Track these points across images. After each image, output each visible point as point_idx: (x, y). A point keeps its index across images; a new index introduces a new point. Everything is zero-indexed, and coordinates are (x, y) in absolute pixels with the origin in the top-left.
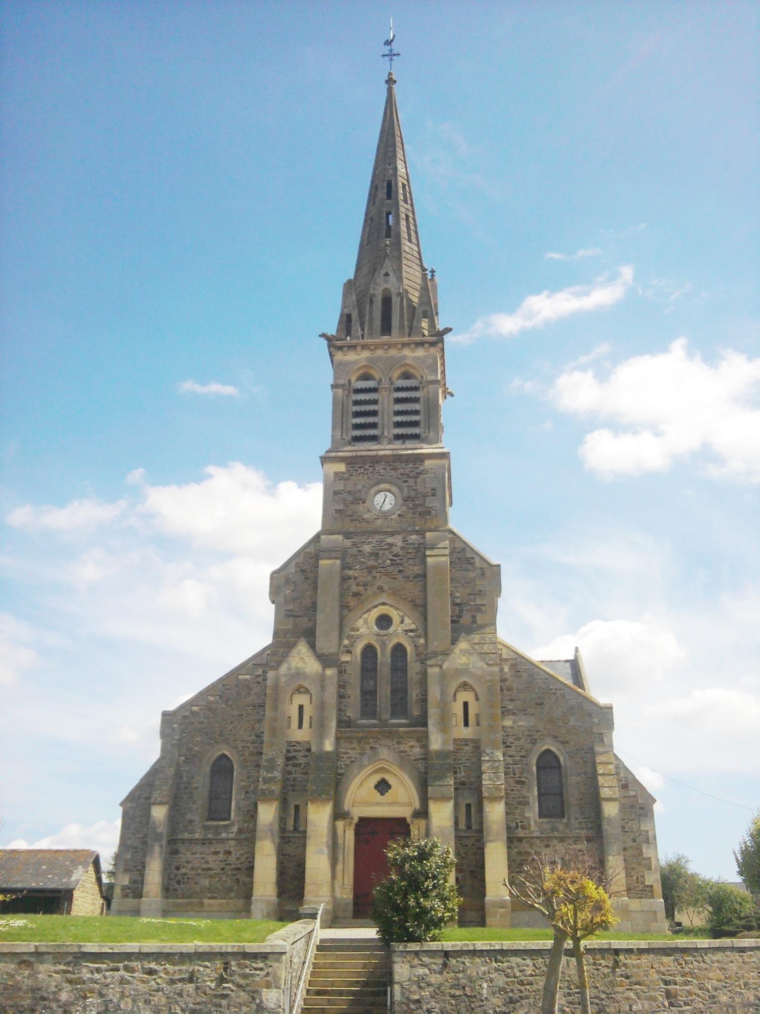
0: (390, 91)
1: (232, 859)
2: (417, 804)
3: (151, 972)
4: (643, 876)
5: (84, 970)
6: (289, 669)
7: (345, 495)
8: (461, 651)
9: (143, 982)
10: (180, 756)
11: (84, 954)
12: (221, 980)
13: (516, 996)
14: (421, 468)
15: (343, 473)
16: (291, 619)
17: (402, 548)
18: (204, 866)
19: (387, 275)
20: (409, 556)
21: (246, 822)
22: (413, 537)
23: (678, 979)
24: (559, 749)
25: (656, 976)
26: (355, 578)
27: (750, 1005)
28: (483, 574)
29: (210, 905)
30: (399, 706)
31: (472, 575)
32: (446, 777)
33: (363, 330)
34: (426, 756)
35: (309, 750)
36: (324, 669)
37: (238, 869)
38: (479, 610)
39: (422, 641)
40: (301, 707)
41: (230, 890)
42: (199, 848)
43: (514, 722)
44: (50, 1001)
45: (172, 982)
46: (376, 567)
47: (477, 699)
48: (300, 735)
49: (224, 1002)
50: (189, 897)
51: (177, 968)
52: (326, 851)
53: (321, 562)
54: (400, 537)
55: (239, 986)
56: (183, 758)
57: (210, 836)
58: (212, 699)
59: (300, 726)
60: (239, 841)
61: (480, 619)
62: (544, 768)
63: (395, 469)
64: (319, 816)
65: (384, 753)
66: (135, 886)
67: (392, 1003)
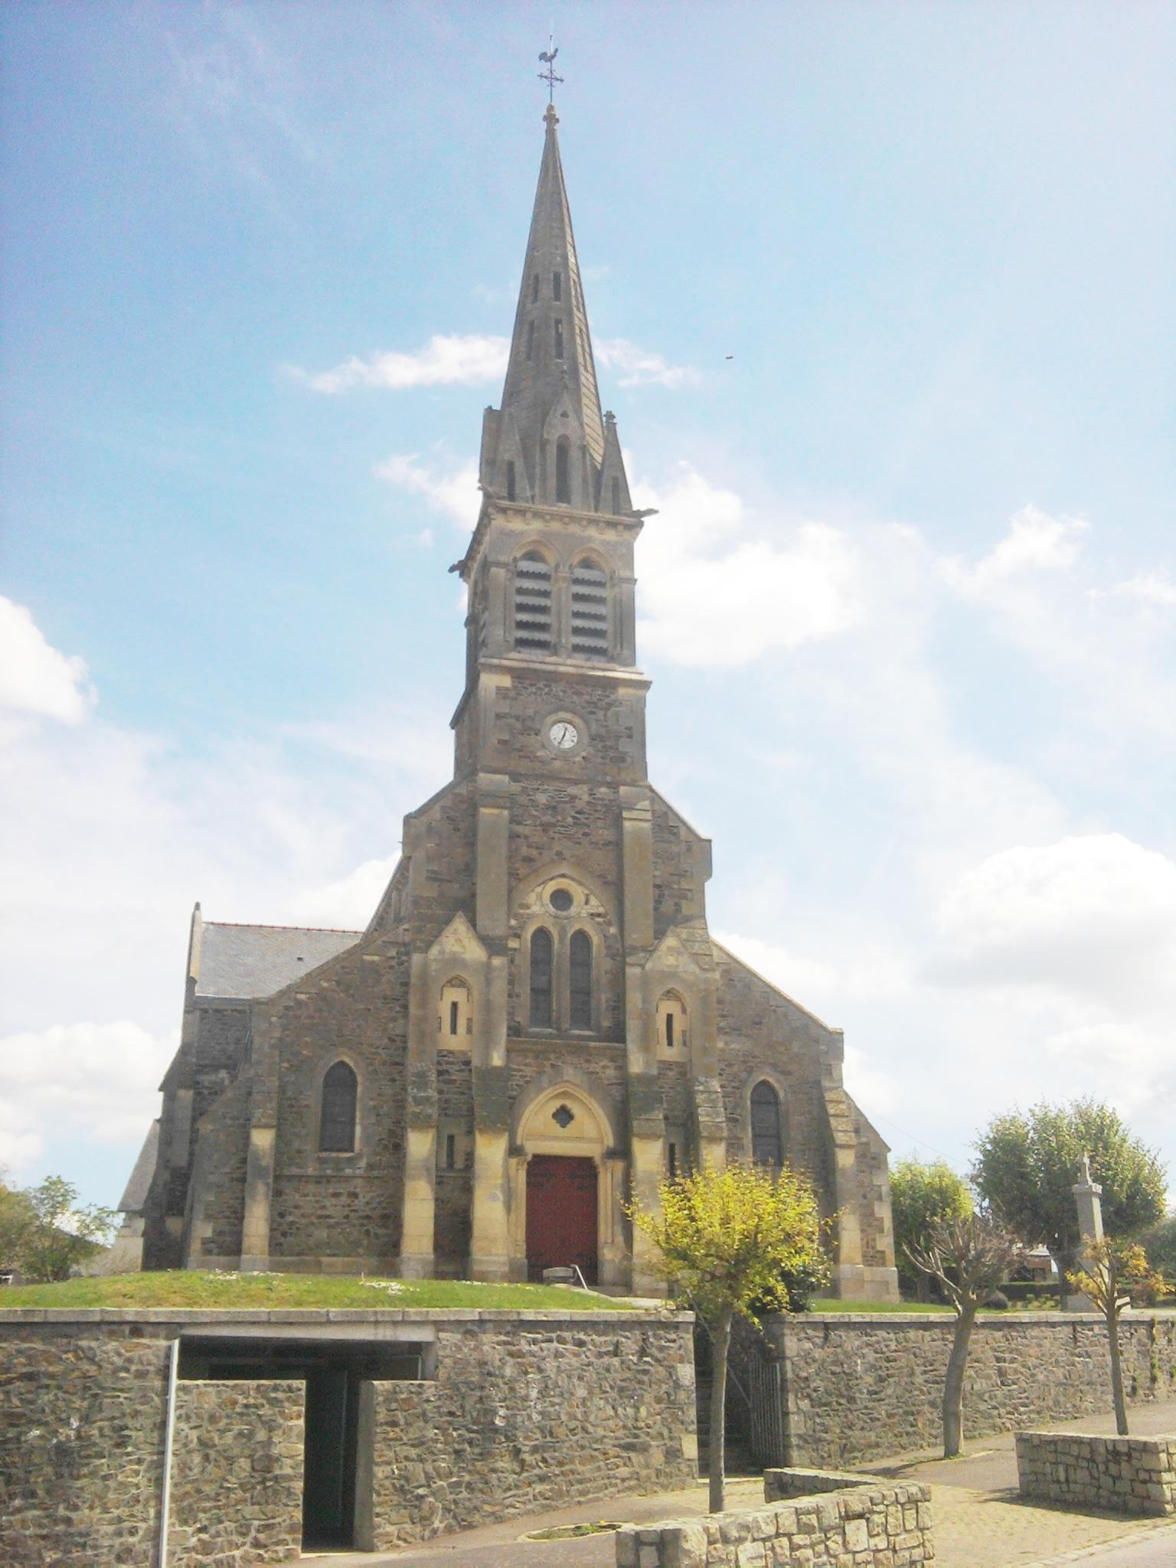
0: (551, 134)
1: (360, 1203)
2: (610, 1141)
3: (581, 1344)
4: (874, 1240)
5: (523, 1342)
6: (442, 952)
7: (511, 721)
8: (670, 949)
9: (576, 1355)
10: (282, 1061)
11: (522, 1321)
12: (643, 1352)
13: (884, 1374)
14: (613, 697)
15: (507, 689)
16: (436, 885)
17: (589, 803)
18: (320, 1212)
19: (564, 415)
20: (597, 815)
21: (377, 1154)
22: (603, 790)
23: (1007, 1356)
24: (778, 1081)
25: (990, 1353)
26: (526, 837)
27: (1061, 1384)
28: (689, 849)
29: (330, 1265)
30: (582, 1014)
31: (675, 849)
32: (653, 1109)
33: (532, 488)
34: (625, 1081)
35: (468, 1063)
36: (490, 957)
37: (368, 1217)
38: (685, 897)
39: (613, 930)
40: (455, 1005)
41: (357, 1244)
42: (311, 1188)
43: (726, 1043)
44: (496, 1376)
45: (600, 1355)
46: (554, 825)
47: (684, 1011)
48: (456, 1042)
49: (646, 1378)
50: (299, 1254)
51: (603, 1339)
52: (500, 1196)
53: (483, 811)
54: (585, 788)
55: (657, 1360)
56: (286, 1065)
57: (329, 1172)
58: (325, 984)
59: (454, 1031)
60: (369, 1179)
61: (686, 909)
62: (759, 1103)
63: (579, 694)
64: (491, 1151)
65: (569, 1073)
66: (221, 1239)
67: (784, 1380)
